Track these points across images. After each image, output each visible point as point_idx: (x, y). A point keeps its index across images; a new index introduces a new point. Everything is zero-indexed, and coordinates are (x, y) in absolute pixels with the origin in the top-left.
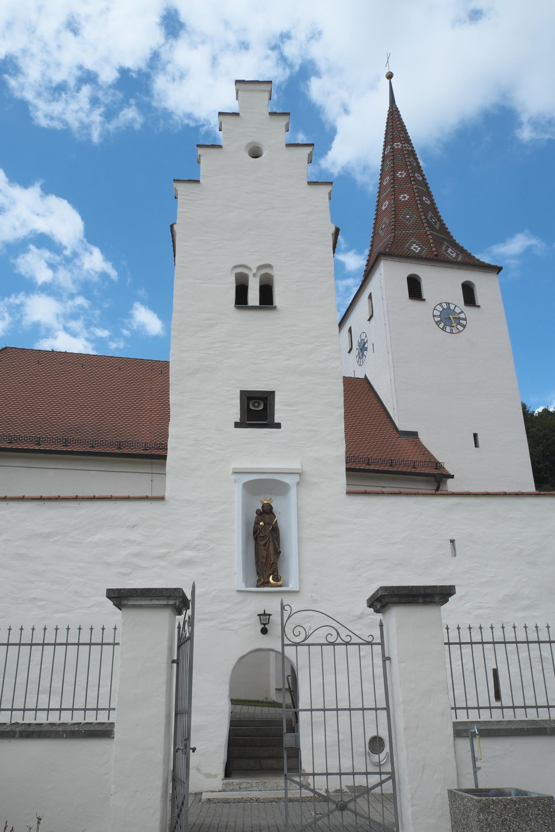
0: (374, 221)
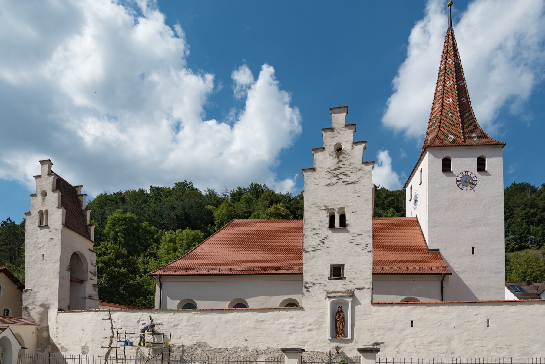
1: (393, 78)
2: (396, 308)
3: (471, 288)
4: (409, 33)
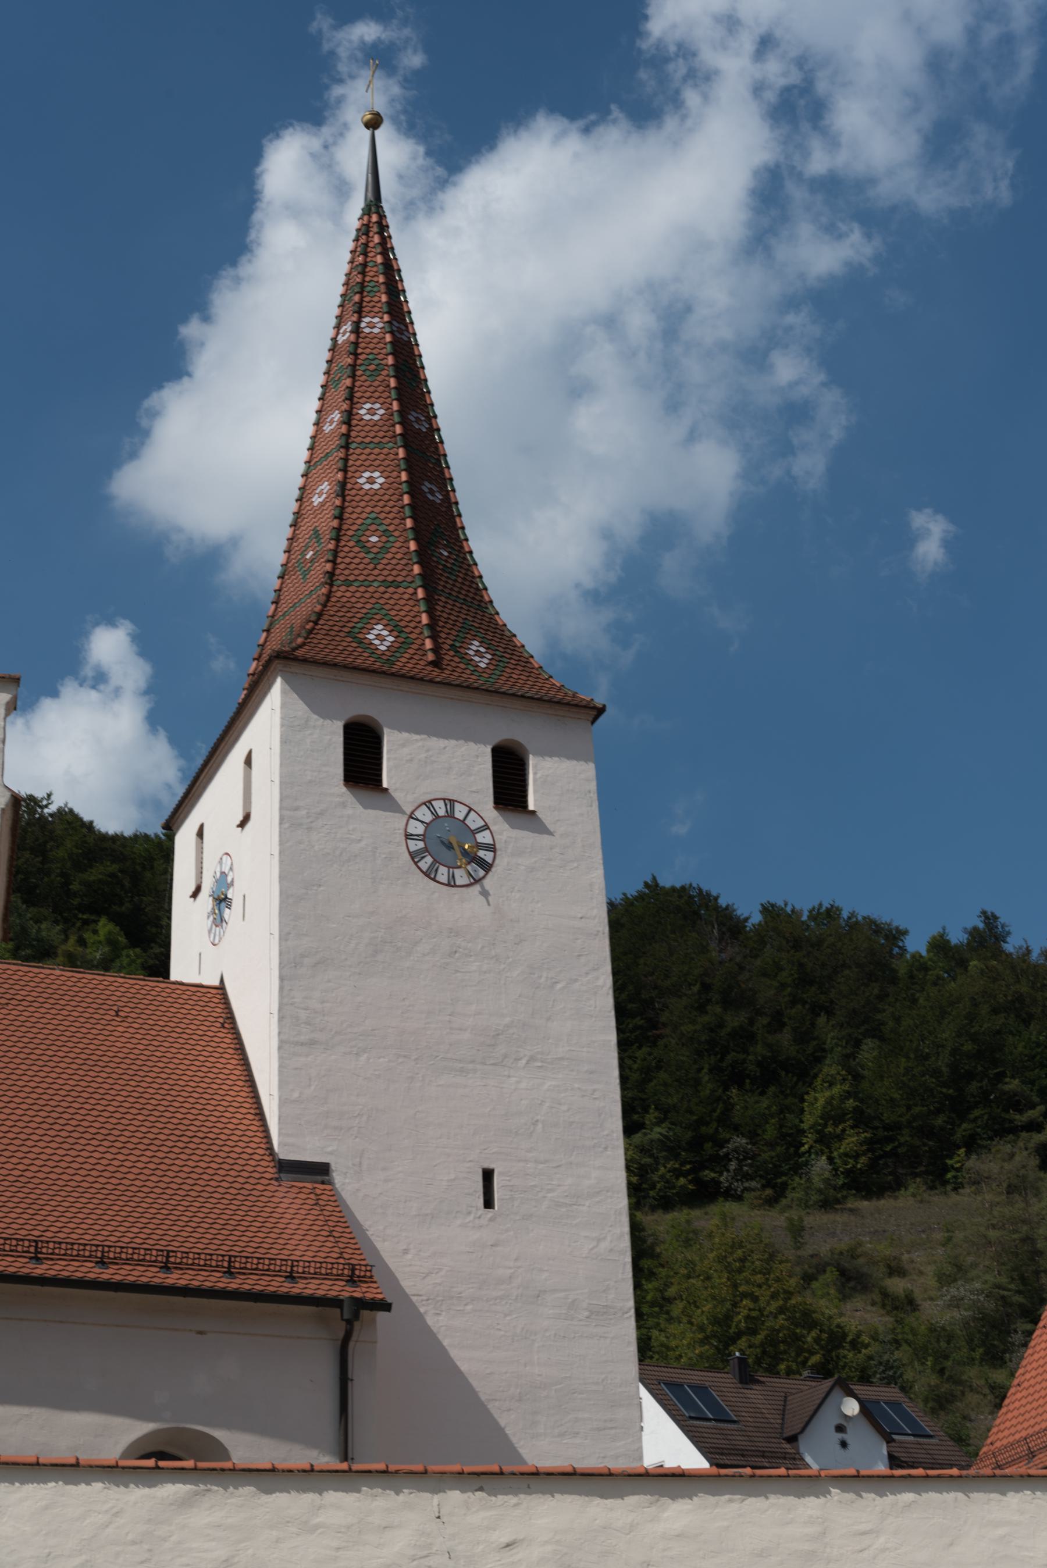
0: (288, 532)
1: (185, 320)
2: (96, 1494)
3: (483, 1390)
4: (256, 156)
